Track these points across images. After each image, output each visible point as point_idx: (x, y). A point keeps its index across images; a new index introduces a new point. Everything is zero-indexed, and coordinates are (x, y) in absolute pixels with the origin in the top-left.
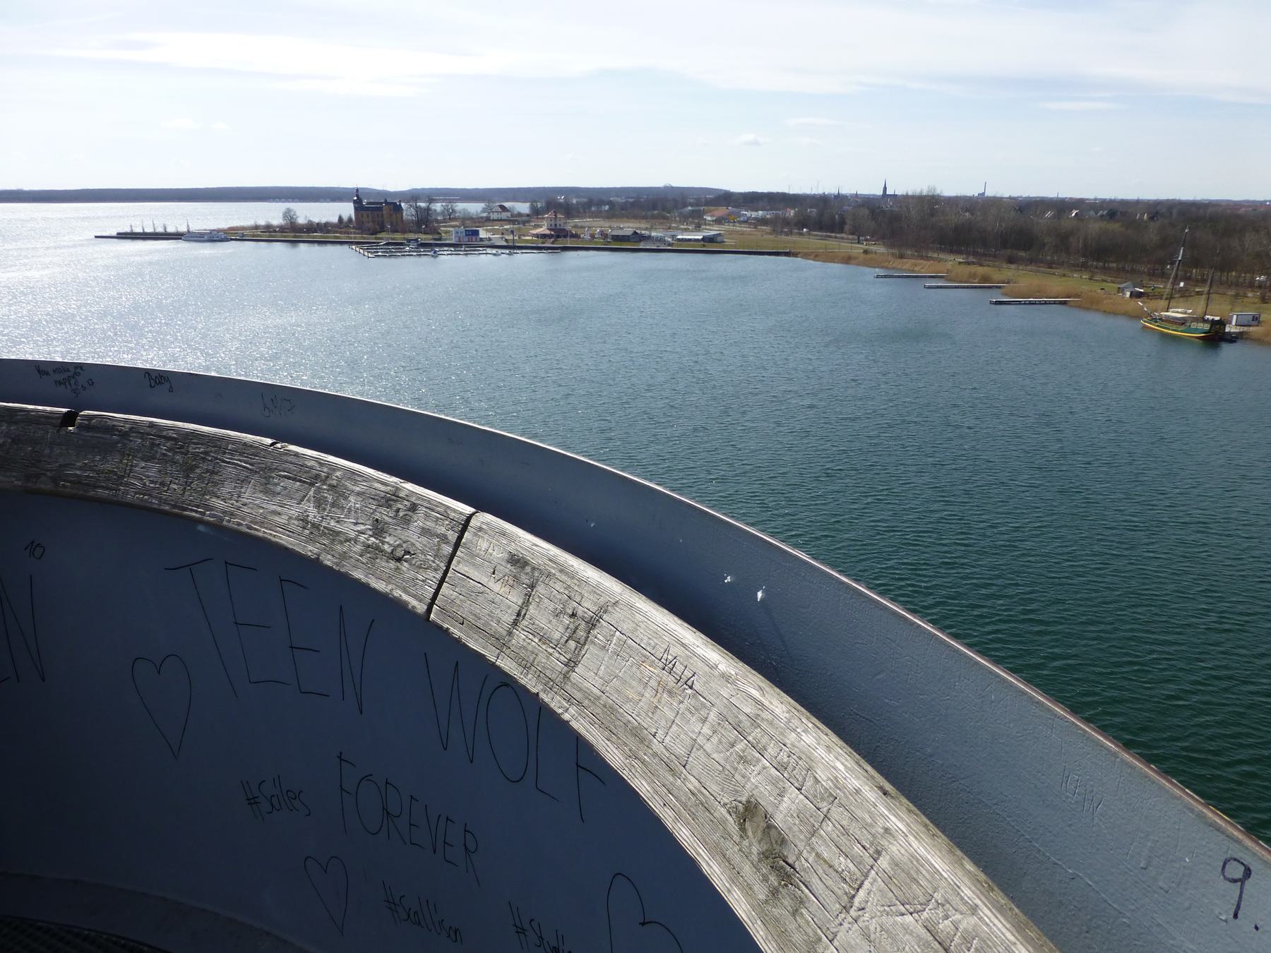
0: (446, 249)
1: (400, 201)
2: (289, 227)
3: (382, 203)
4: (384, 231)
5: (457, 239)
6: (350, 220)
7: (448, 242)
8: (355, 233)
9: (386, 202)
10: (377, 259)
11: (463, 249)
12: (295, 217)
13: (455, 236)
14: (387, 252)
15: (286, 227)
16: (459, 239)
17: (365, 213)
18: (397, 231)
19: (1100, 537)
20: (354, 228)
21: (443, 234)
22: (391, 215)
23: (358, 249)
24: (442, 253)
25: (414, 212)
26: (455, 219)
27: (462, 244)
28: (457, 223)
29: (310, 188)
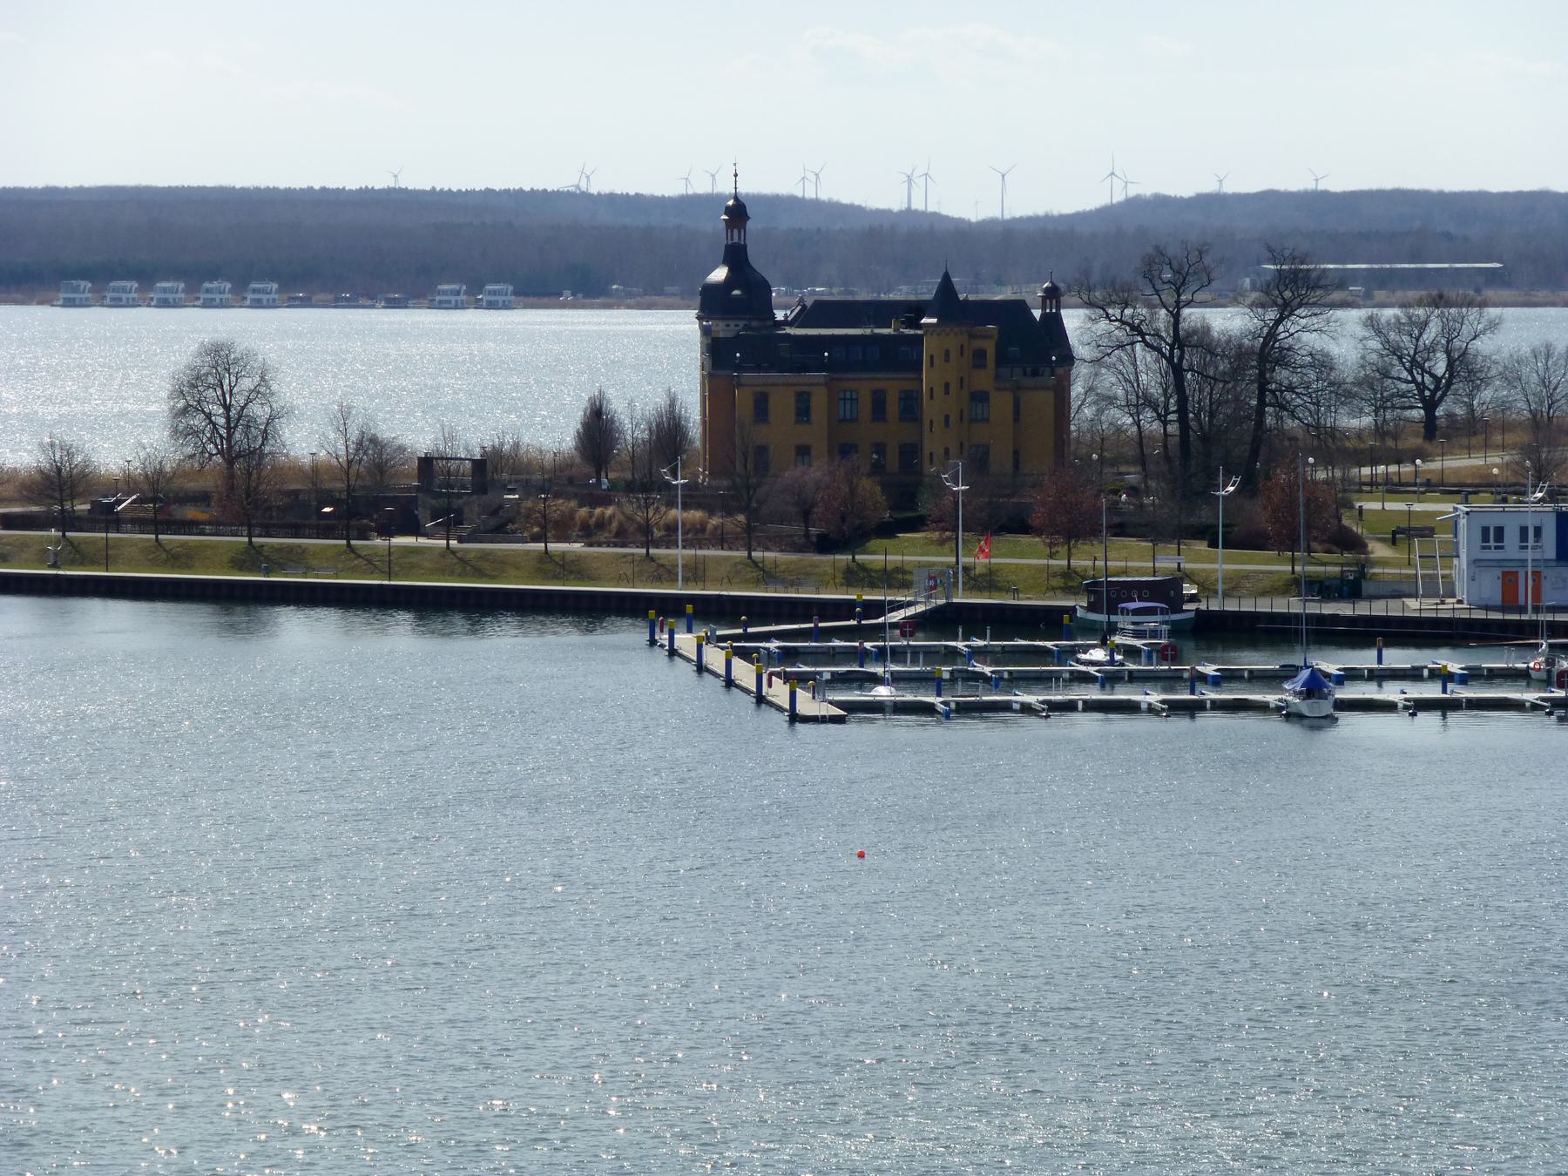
0: (1397, 658)
1: (1053, 295)
2: (208, 483)
3: (918, 309)
4: (914, 525)
5: (1491, 588)
6: (668, 435)
7: (1413, 606)
8: (697, 535)
9: (947, 300)
10: (857, 732)
11: (1536, 662)
12: (259, 411)
13: (1475, 563)
14: (938, 685)
15: (192, 486)
16: (1509, 581)
17: (781, 388)
18: (1019, 525)
19: (359, 818)
20: (693, 496)
21: (1379, 550)
22: (980, 397)
23: (715, 657)
24: (1367, 691)
25: (1149, 370)
26: (1473, 431)
27: (1532, 629)
28: (1493, 462)
29: (367, 199)
